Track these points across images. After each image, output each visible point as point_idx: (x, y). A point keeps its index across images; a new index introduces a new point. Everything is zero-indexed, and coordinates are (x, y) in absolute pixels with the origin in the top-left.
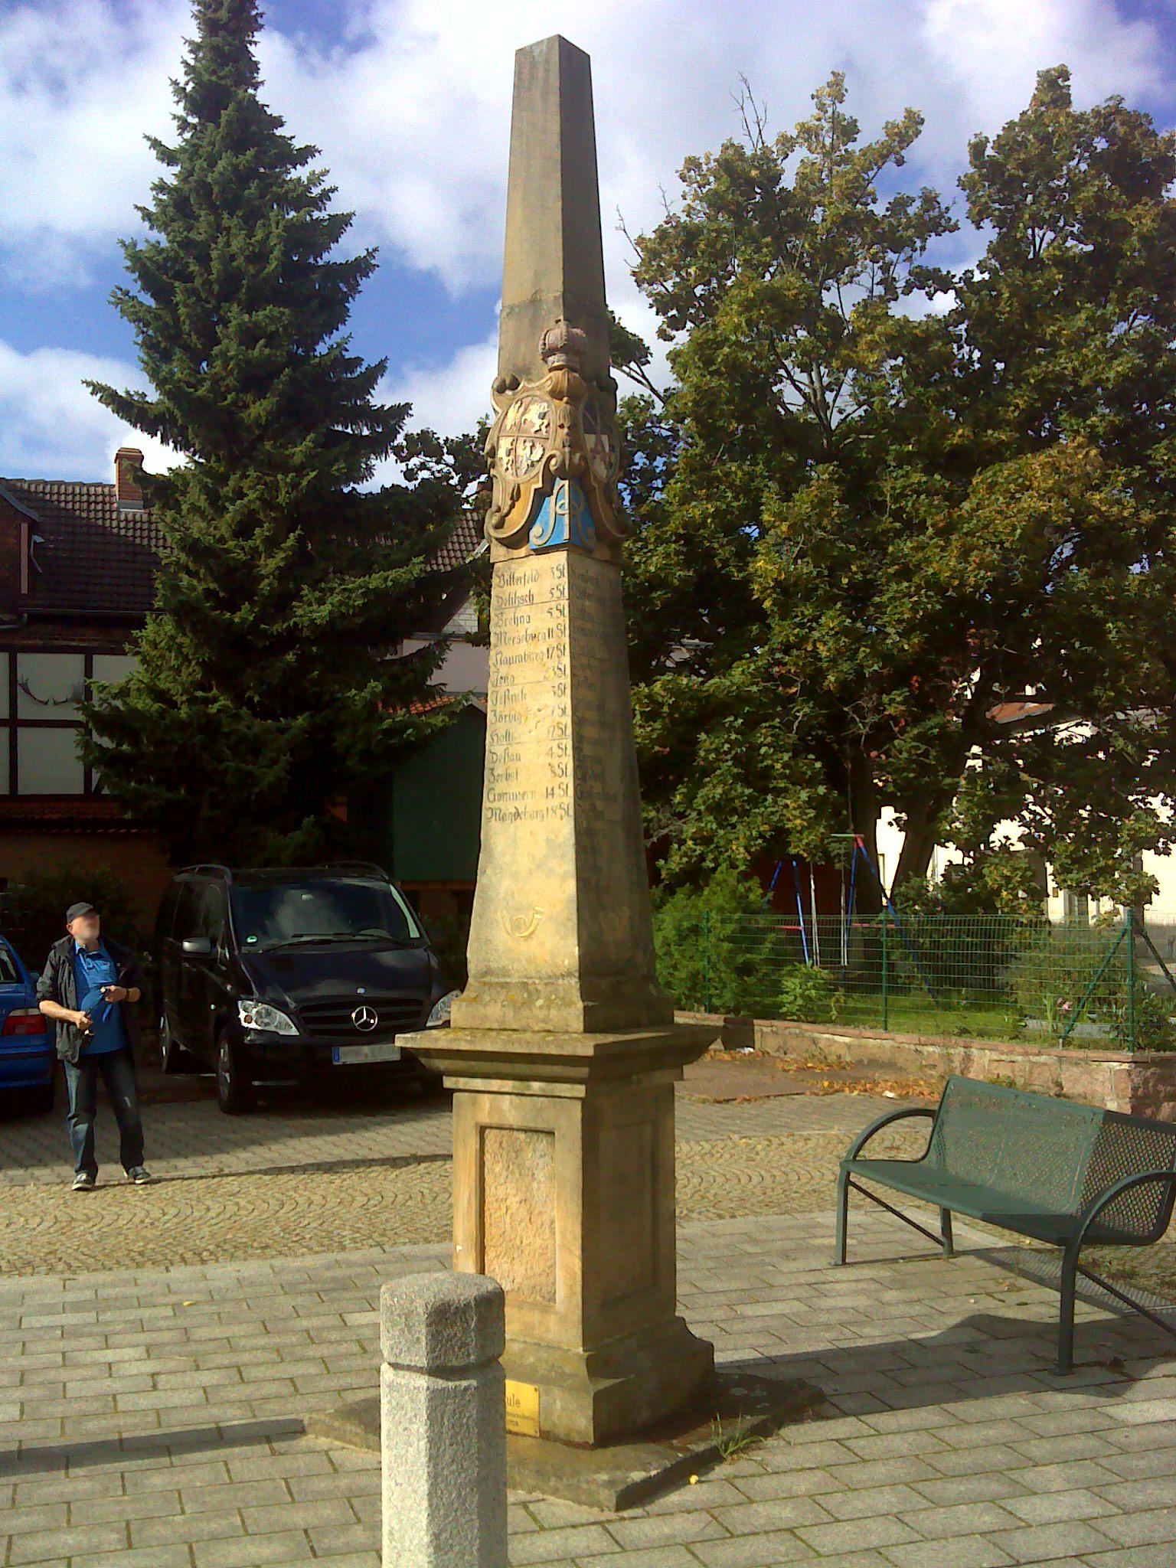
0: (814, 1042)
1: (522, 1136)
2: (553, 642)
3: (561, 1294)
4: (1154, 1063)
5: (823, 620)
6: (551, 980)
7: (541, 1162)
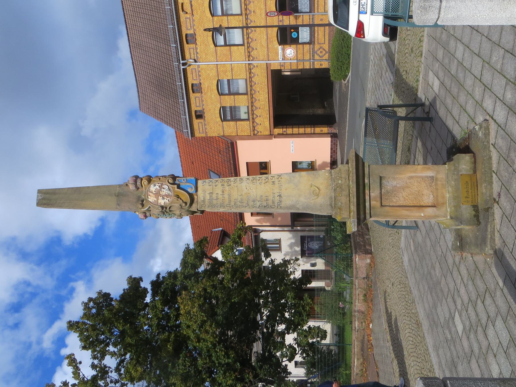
0: (357, 374)
1: (383, 190)
2: (226, 184)
3: (430, 174)
4: (356, 249)
5: (220, 381)
6: (333, 180)
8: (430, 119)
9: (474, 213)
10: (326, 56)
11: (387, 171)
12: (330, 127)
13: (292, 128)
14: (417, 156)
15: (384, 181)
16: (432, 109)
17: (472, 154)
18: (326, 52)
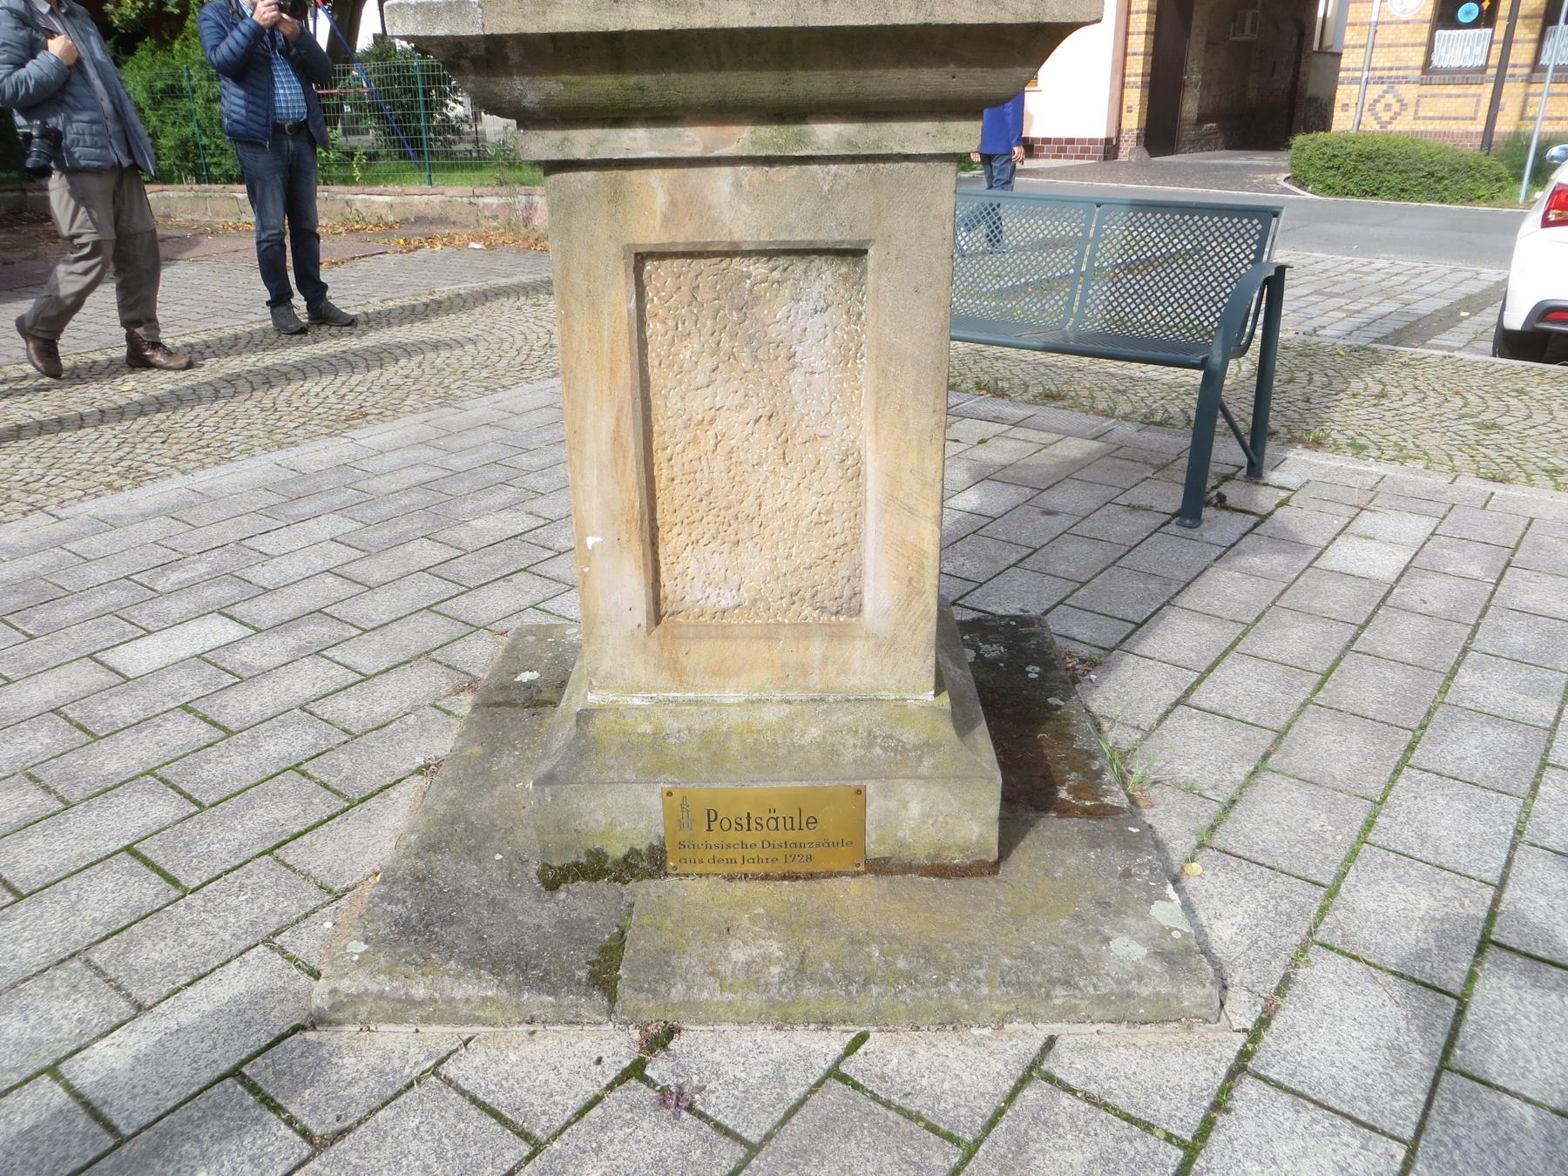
1: (759, 268)
7: (816, 324)
8: (1192, 509)
9: (616, 851)
10: (1370, 125)
11: (902, 305)
12: (1138, 137)
13: (1149, 11)
14: (1020, 433)
15: (827, 274)
16: (1242, 523)
17: (993, 855)
18: (1384, 125)
